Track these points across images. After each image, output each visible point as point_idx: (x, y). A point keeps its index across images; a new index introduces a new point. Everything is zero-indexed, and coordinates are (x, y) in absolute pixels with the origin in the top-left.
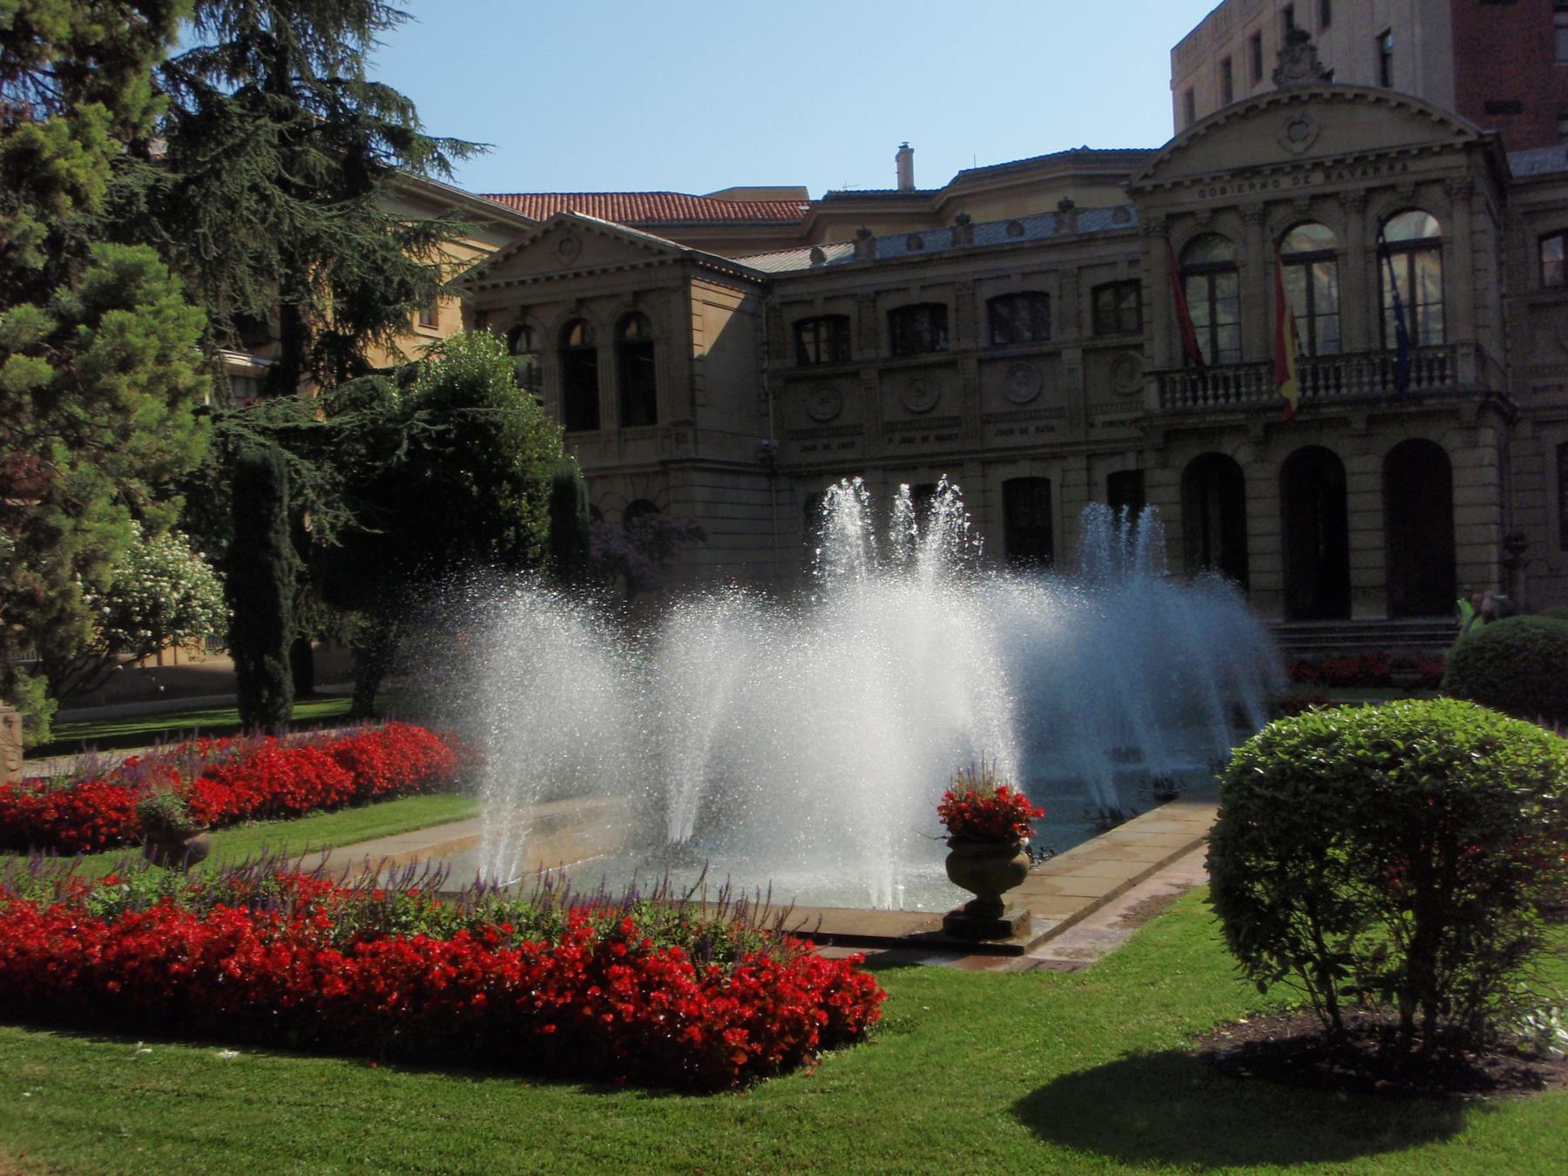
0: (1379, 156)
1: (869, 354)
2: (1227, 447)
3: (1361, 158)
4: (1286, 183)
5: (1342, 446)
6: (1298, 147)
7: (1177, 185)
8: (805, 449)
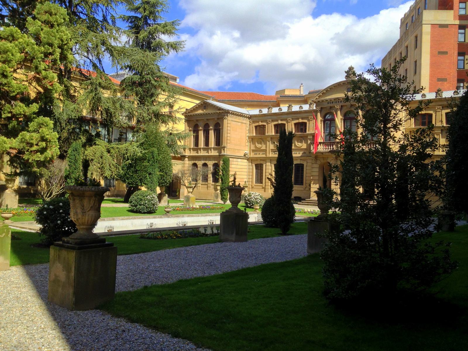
1: (270, 134)
8: (255, 154)
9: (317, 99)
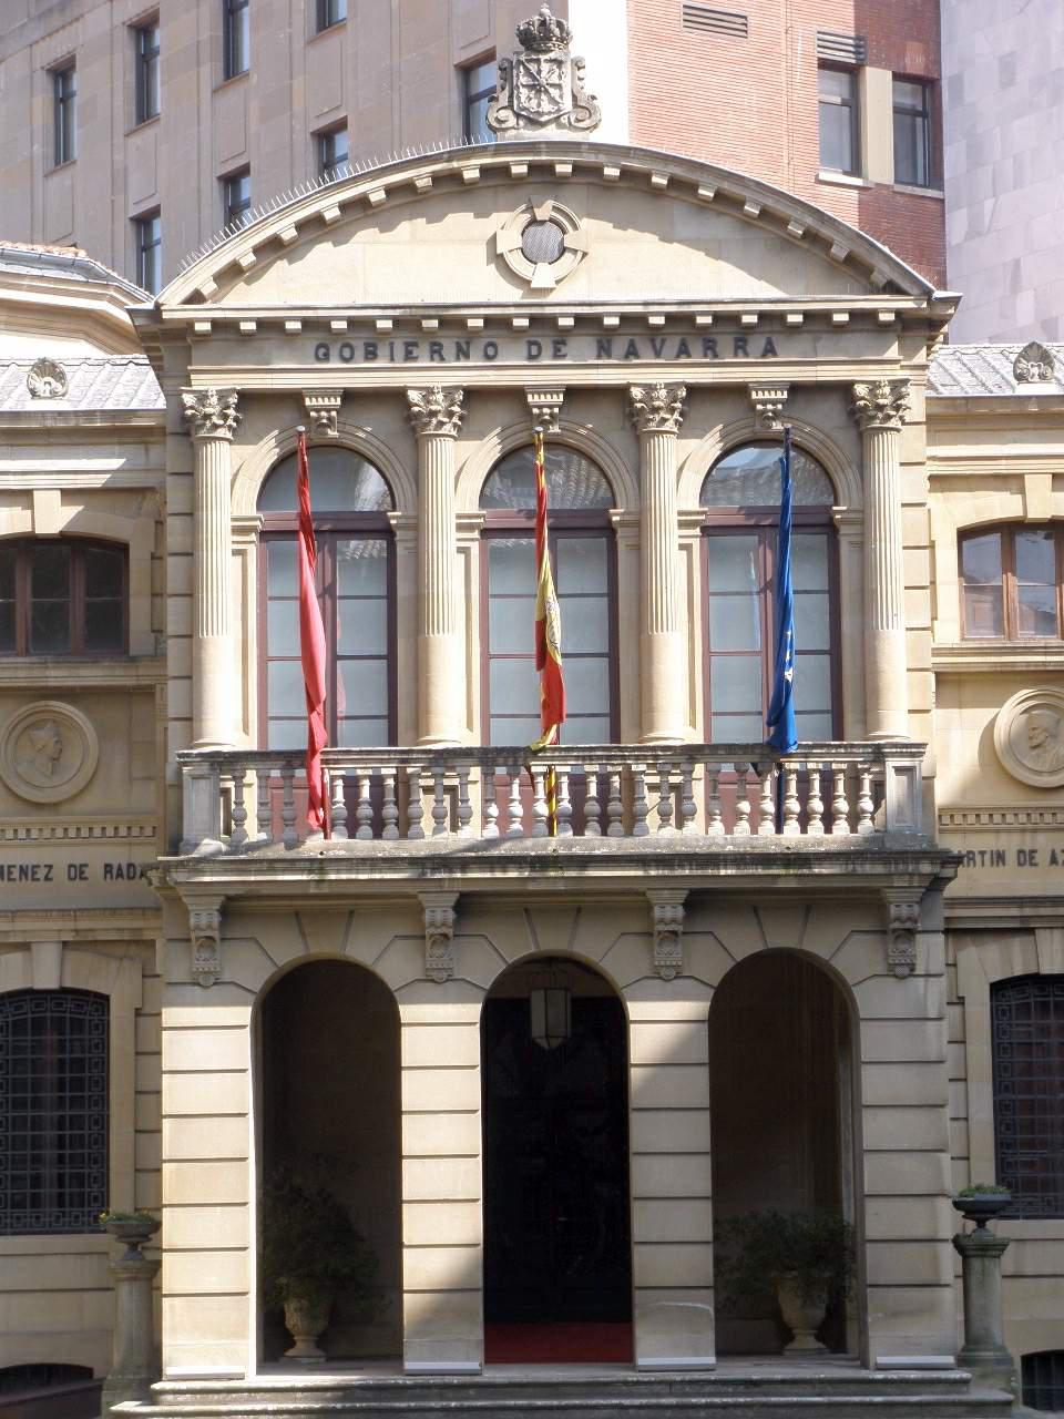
0: (718, 318)
2: (362, 948)
3: (680, 321)
4: (513, 355)
5: (391, 962)
6: (542, 275)
7: (270, 327)
9: (196, 298)
